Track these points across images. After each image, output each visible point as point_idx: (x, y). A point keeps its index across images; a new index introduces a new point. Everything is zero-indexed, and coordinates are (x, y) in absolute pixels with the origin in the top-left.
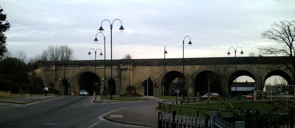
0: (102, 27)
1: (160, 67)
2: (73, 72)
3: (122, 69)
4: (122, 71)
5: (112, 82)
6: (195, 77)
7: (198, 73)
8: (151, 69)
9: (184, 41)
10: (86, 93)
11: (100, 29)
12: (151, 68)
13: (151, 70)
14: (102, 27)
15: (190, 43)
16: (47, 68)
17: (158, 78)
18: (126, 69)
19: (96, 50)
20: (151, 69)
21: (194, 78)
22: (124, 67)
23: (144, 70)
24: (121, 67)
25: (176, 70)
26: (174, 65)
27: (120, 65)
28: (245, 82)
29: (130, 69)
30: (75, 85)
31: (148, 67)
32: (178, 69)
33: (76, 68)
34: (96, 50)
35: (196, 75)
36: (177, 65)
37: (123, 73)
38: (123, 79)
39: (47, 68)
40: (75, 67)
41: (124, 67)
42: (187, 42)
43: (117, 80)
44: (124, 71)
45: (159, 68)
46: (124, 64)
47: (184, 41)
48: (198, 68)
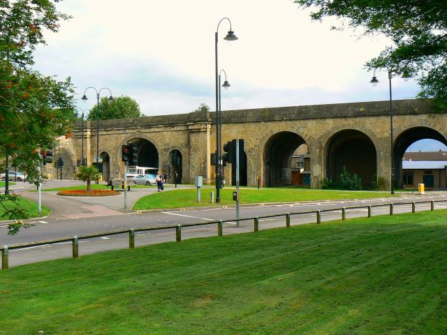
0: (233, 33)
1: (259, 124)
2: (117, 139)
3: (191, 132)
4: (191, 135)
5: (176, 155)
6: (326, 142)
7: (332, 135)
8: (243, 130)
9: (216, 34)
10: (23, 177)
11: (228, 36)
12: (244, 127)
13: (242, 131)
14: (233, 33)
15: (231, 36)
16: (78, 134)
17: (256, 146)
18: (199, 131)
19: (98, 91)
20: (243, 130)
21: (323, 144)
22: (196, 127)
23: (230, 132)
24: (190, 128)
25: (289, 130)
26: (286, 120)
27: (188, 124)
28: (438, 151)
29: (205, 130)
30: (116, 159)
31: (238, 126)
32: (292, 127)
33: (120, 132)
34: (98, 91)
35: (327, 140)
36: (290, 120)
37: (193, 138)
38: (194, 149)
39: (78, 134)
40: (119, 130)
41: (196, 127)
42: (223, 34)
43: (183, 151)
44: (194, 134)
45: (257, 128)
46: (195, 123)
47: (216, 34)
48: (332, 125)
